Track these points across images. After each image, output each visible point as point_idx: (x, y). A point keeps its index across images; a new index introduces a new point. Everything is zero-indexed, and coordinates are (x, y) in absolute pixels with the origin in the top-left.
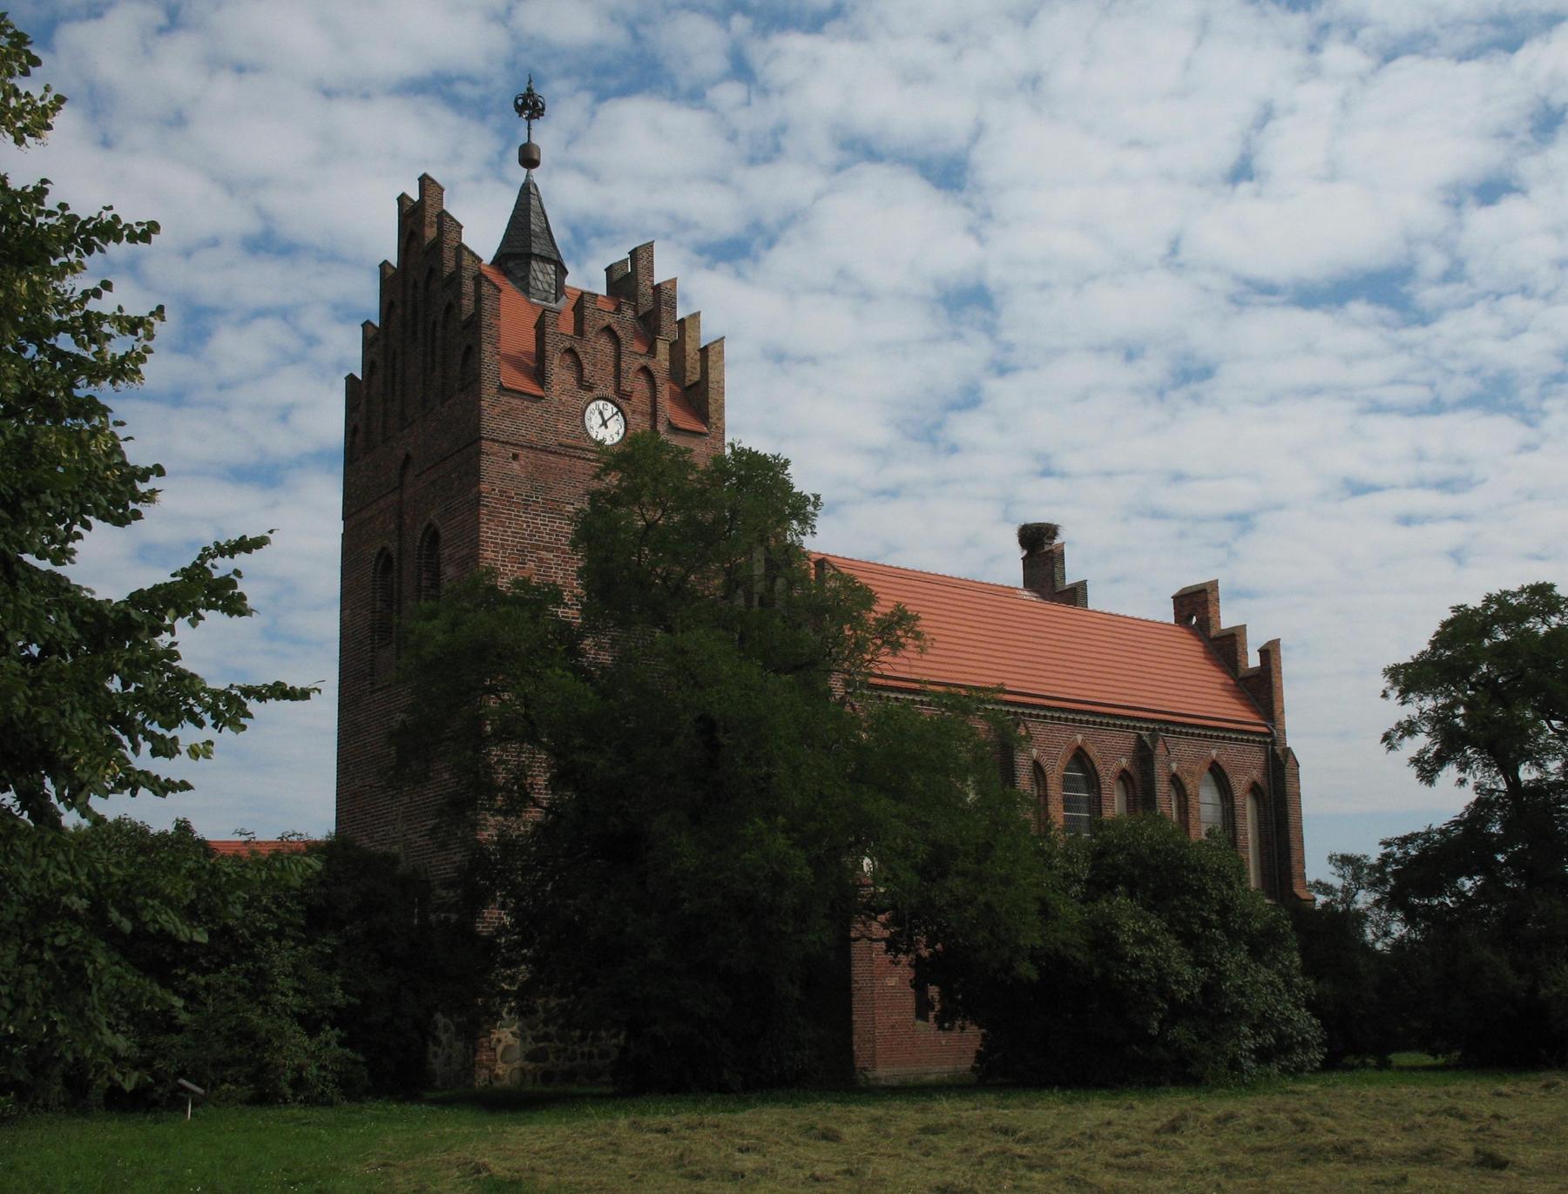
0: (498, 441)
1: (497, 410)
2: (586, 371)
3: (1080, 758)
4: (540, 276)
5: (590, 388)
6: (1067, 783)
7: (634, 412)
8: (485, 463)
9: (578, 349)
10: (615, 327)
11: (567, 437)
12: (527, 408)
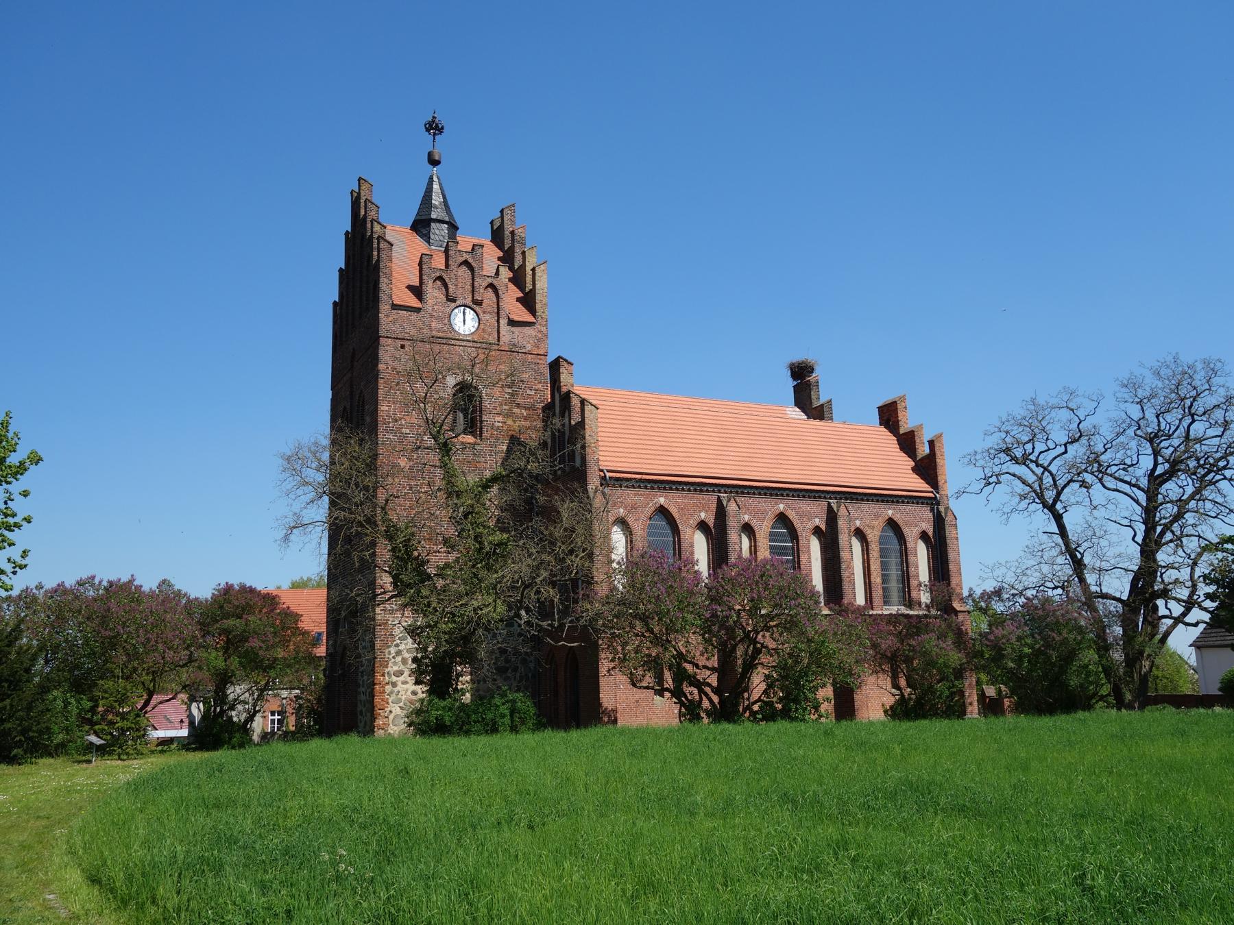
0: (391, 338)
1: (390, 319)
2: (450, 290)
3: (782, 519)
4: (437, 232)
5: (454, 300)
6: (773, 537)
7: (484, 312)
8: (381, 350)
9: (445, 277)
10: (470, 261)
11: (439, 331)
12: (410, 315)
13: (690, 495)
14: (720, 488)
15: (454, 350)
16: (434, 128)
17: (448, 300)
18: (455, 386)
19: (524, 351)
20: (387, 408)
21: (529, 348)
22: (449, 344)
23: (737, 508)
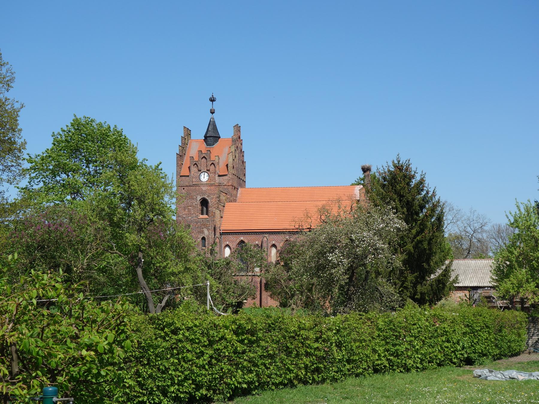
13: (253, 236)
16: (212, 100)
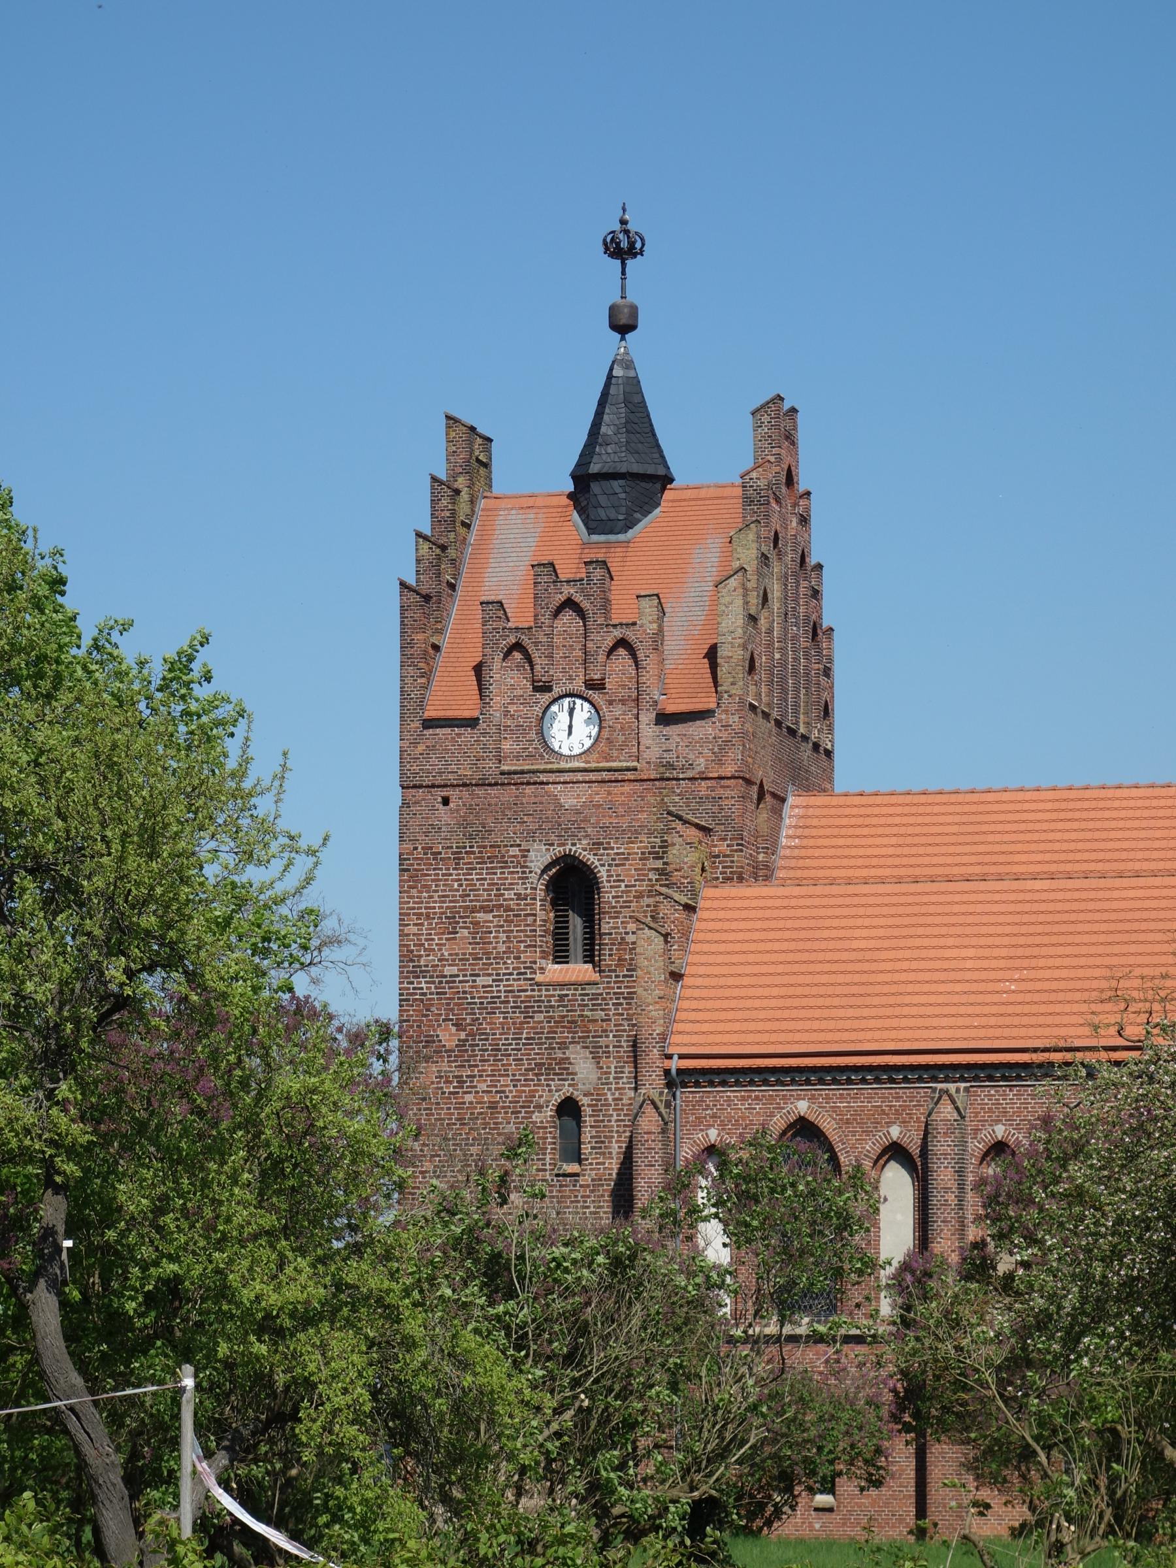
1: (421, 748)
2: (538, 668)
7: (611, 703)
10: (578, 598)
11: (517, 758)
12: (459, 735)
14: (936, 1073)
15: (548, 794)
17: (536, 689)
18: (544, 871)
19: (690, 774)
20: (415, 929)
21: (701, 764)
22: (535, 783)
23: (956, 1116)
